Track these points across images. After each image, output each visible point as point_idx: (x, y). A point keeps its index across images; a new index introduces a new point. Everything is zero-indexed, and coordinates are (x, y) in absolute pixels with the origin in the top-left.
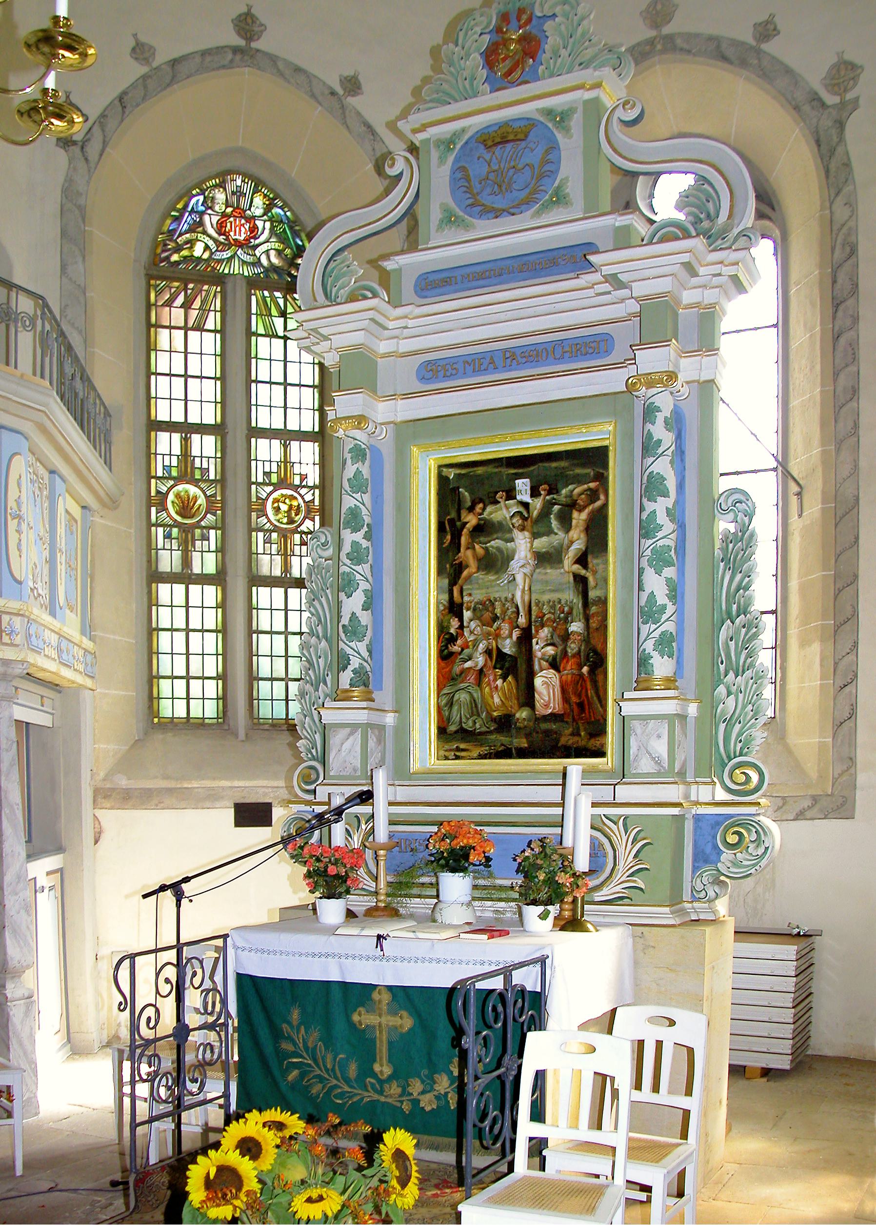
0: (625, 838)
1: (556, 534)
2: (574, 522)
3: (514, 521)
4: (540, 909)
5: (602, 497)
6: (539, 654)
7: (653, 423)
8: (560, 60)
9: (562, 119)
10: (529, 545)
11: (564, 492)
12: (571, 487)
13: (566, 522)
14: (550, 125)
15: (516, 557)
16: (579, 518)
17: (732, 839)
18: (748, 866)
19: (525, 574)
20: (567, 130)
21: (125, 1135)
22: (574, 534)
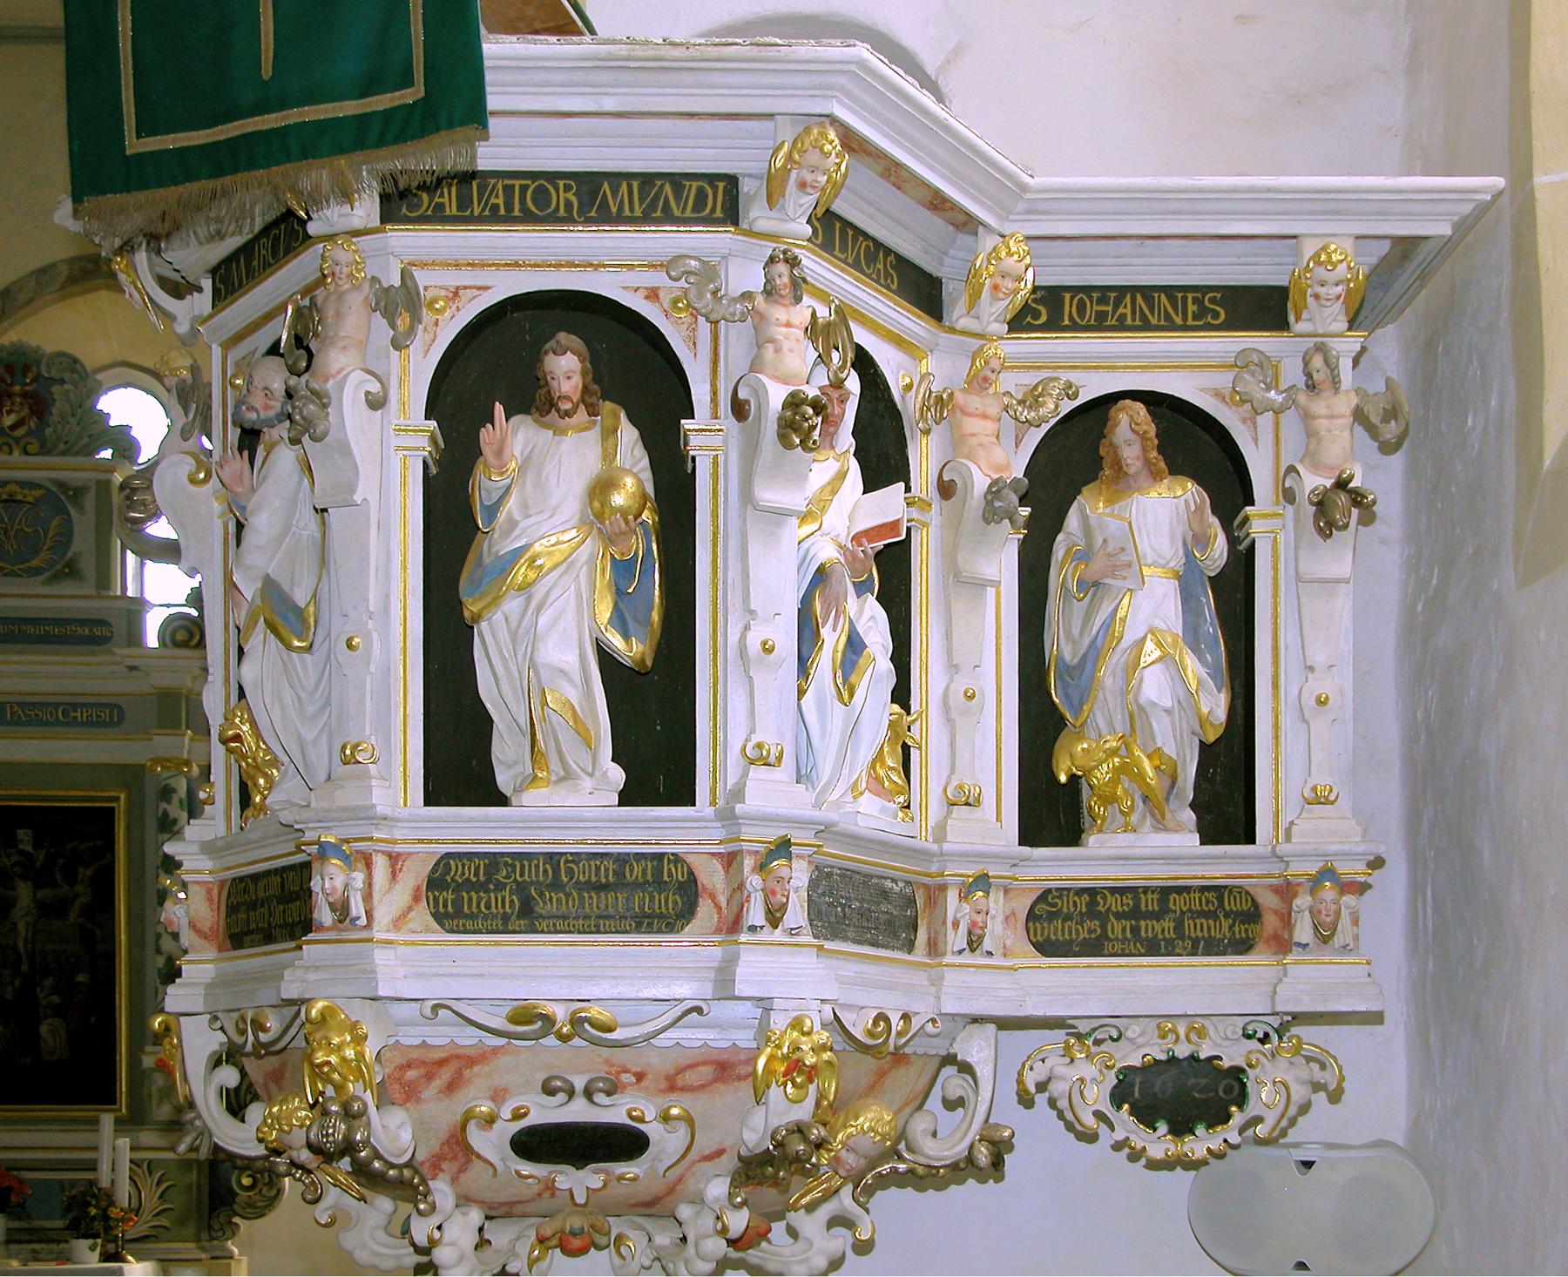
0: (149, 1181)
1: (60, 887)
2: (80, 877)
3: (16, 869)
4: (90, 1242)
5: (109, 855)
6: (44, 1002)
7: (169, 803)
8: (68, 426)
9: (75, 494)
10: (31, 894)
11: (69, 846)
12: (75, 843)
13: (72, 880)
14: (63, 498)
15: (18, 906)
16: (86, 873)
17: (246, 1181)
18: (262, 1207)
19: (28, 923)
20: (80, 507)
21: (925, 927)
22: (79, 888)
